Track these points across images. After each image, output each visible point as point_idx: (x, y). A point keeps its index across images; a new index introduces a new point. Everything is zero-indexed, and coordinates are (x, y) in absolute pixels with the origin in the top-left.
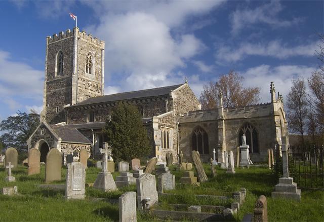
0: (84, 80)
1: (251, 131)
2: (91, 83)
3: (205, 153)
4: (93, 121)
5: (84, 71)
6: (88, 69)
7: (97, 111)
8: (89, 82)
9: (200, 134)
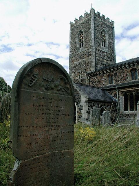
0: (101, 52)
4: (112, 83)
6: (103, 43)
7: (116, 73)
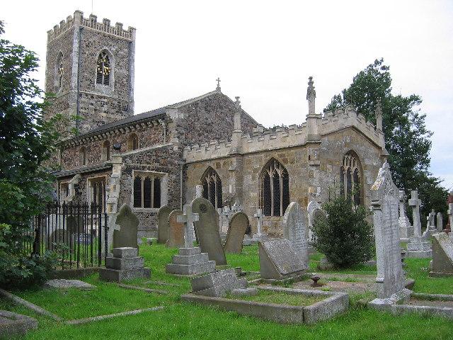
1: (280, 172)
2: (106, 100)
3: (274, 215)
5: (92, 82)
8: (103, 100)
9: (212, 182)
